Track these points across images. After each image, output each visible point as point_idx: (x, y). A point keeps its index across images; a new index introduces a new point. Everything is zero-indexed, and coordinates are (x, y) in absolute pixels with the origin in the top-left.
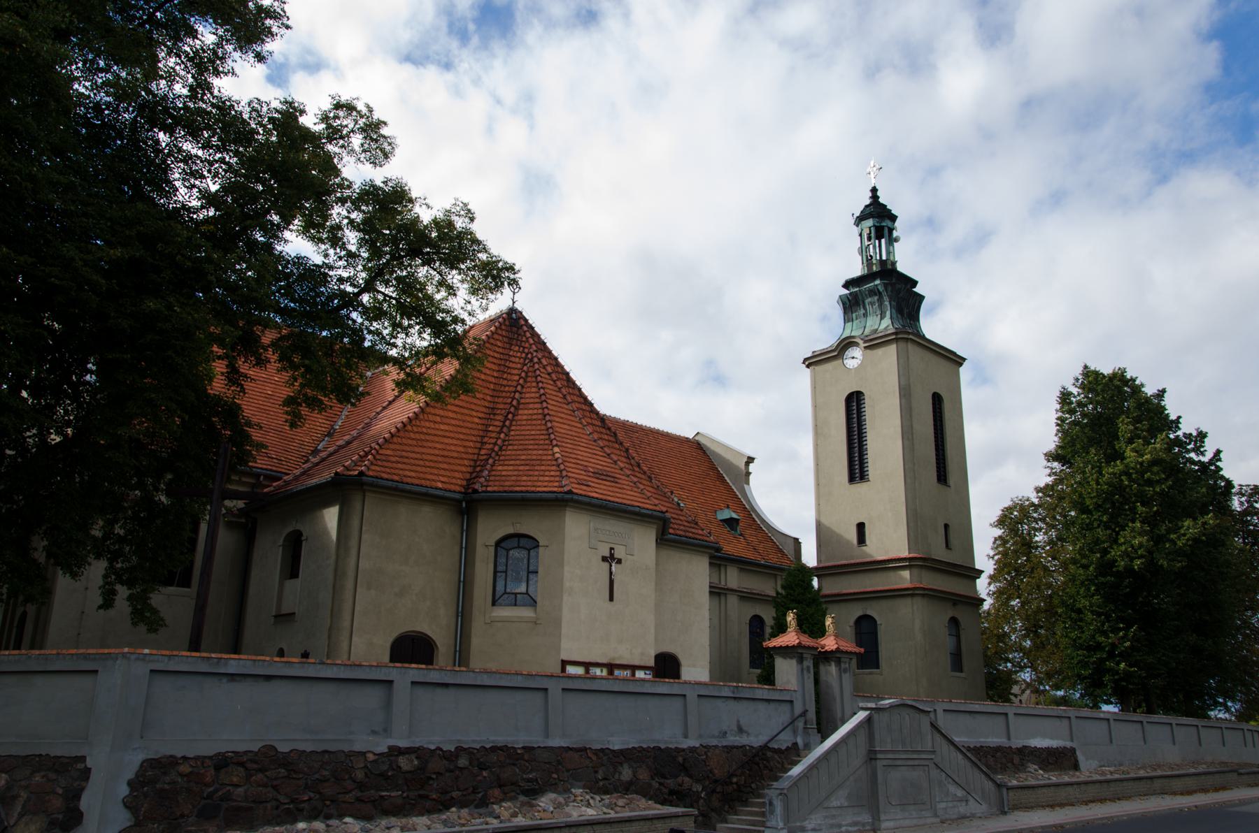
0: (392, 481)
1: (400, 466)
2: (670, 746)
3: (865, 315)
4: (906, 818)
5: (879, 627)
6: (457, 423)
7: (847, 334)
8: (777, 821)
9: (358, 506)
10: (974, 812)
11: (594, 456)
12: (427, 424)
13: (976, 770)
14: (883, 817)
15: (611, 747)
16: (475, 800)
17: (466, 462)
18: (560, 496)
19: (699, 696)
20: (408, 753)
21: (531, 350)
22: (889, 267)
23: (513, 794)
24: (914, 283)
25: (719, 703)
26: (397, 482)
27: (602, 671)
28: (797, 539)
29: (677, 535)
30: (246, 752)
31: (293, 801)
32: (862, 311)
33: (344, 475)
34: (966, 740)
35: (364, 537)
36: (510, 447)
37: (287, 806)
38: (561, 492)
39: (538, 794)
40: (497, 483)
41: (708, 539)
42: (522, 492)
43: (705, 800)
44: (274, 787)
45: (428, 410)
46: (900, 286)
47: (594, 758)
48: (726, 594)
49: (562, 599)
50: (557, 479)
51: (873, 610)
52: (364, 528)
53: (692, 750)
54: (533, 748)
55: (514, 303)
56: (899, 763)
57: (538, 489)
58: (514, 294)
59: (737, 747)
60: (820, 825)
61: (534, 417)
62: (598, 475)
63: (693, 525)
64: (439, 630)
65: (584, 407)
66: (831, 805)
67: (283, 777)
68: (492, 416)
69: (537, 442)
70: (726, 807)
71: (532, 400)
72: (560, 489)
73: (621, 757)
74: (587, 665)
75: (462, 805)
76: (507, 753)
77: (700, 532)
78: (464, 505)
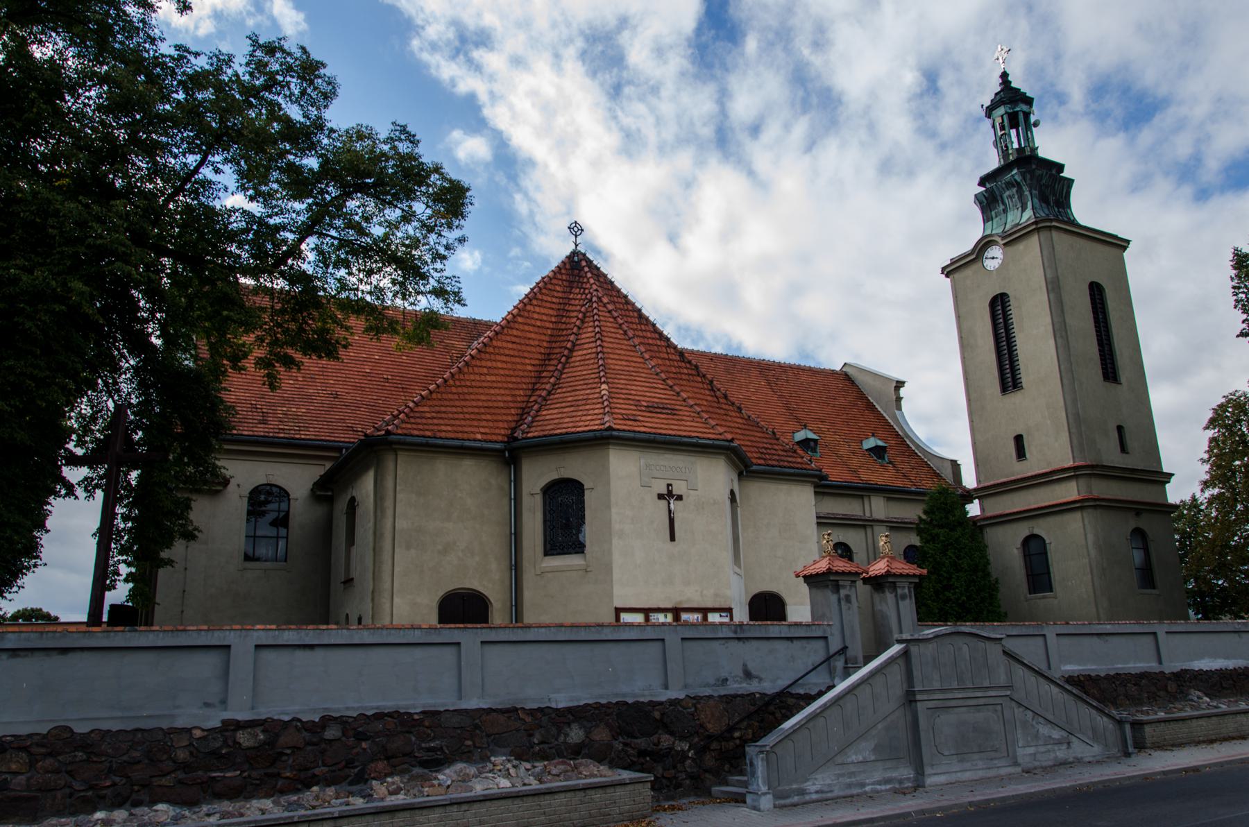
0: (424, 436)
1: (436, 421)
2: (642, 700)
3: (1005, 211)
4: (966, 770)
5: (1048, 546)
6: (507, 372)
7: (988, 232)
8: (758, 785)
9: (391, 465)
10: (1080, 756)
11: (652, 390)
12: (472, 377)
13: (1080, 704)
14: (928, 770)
15: (553, 705)
16: (349, 776)
17: (513, 411)
18: (598, 434)
19: (683, 639)
20: (250, 727)
21: (591, 291)
22: (1028, 153)
23: (405, 766)
24: (1060, 167)
25: (716, 644)
26: (429, 437)
27: (666, 617)
28: (956, 461)
29: (768, 465)
30: (30, 736)
31: (91, 788)
32: (1002, 207)
33: (373, 436)
34: (1093, 667)
35: (399, 496)
36: (559, 391)
37: (82, 794)
38: (601, 430)
39: (443, 764)
40: (539, 428)
41: (808, 467)
42: (561, 434)
43: (693, 760)
44: (68, 773)
45: (474, 362)
46: (1040, 172)
47: (529, 719)
48: (872, 526)
49: (611, 543)
50: (600, 416)
51: (1041, 528)
52: (398, 488)
53: (674, 702)
54: (438, 713)
55: (576, 246)
56: (953, 703)
57: (578, 430)
58: (576, 236)
59: (742, 696)
60: (829, 785)
61: (588, 357)
62: (651, 408)
63: (790, 454)
64: (492, 586)
65: (658, 342)
66: (849, 760)
67: (81, 761)
68: (547, 362)
69: (586, 382)
70: (727, 767)
71: (588, 340)
72: (602, 427)
73: (570, 716)
74: (646, 612)
75: (329, 783)
76: (402, 721)
77: (799, 460)
78: (507, 455)
